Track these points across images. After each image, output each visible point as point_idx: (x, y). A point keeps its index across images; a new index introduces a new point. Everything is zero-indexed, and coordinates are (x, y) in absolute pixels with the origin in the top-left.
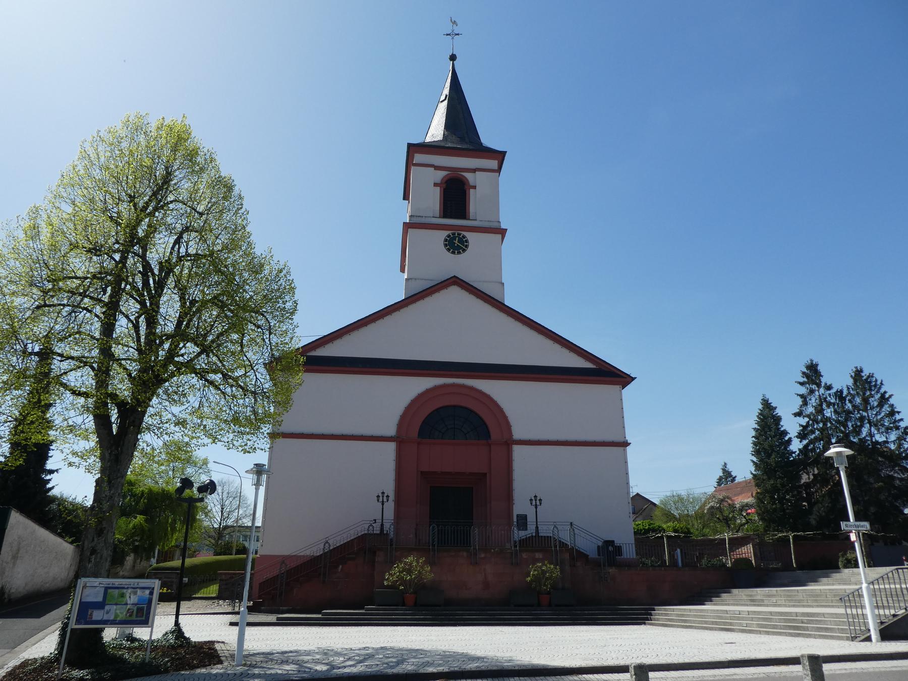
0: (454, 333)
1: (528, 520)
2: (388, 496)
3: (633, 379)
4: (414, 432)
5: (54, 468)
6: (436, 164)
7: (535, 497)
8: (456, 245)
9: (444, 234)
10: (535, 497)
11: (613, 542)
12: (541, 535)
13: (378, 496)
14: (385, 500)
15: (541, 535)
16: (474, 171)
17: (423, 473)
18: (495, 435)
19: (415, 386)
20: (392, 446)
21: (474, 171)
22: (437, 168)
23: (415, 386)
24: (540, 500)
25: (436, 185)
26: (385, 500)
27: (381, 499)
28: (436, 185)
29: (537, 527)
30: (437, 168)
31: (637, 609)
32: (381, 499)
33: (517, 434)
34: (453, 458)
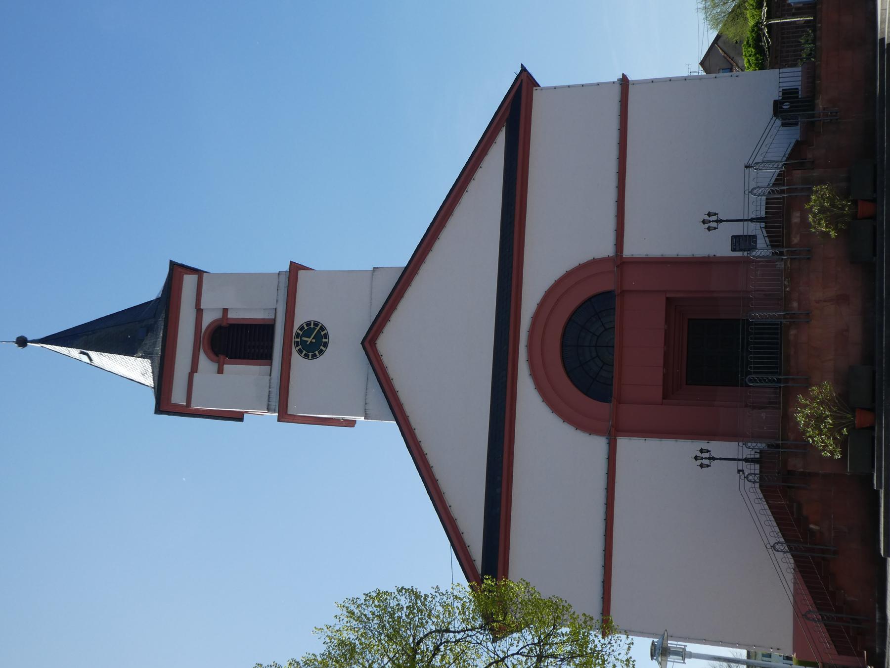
0: (449, 346)
3: (524, 69)
4: (603, 409)
6: (188, 369)
7: (696, 458)
8: (313, 340)
9: (297, 359)
10: (704, 222)
11: (776, 102)
12: (758, 456)
14: (714, 218)
15: (763, 214)
16: (199, 311)
17: (665, 396)
18: (607, 284)
20: (624, 444)
21: (199, 311)
22: (194, 368)
24: (709, 215)
25: (220, 371)
28: (220, 371)
29: (752, 220)
30: (194, 368)
33: (607, 249)
34: (642, 349)
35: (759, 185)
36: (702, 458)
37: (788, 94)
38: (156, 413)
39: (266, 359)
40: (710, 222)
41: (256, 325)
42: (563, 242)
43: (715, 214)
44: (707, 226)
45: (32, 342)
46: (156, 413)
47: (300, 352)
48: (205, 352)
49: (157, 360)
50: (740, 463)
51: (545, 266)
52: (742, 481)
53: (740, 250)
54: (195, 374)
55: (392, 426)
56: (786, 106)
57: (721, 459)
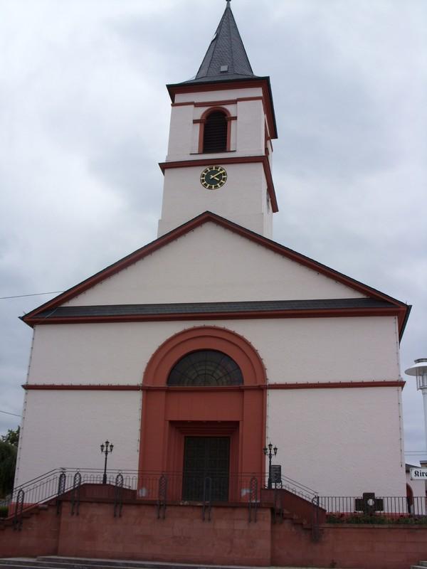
0: (213, 274)
1: (283, 472)
2: (112, 446)
3: (22, 318)
4: (163, 384)
5: (17, 429)
6: (196, 101)
7: (107, 443)
9: (200, 171)
10: (107, 443)
11: (373, 494)
12: (108, 483)
13: (102, 446)
14: (273, 452)
16: (234, 102)
17: (171, 422)
19: (165, 331)
20: (138, 396)
21: (234, 102)
23: (165, 331)
24: (275, 449)
25: (235, 118)
26: (273, 452)
27: (105, 449)
28: (195, 122)
31: (64, 561)
32: (105, 449)
33: (272, 378)
35: (125, 480)
36: (107, 446)
37: (379, 503)
38: (269, 77)
40: (270, 449)
41: (226, 145)
42: (280, 350)
43: (275, 453)
44: (105, 444)
45: (228, 4)
46: (269, 77)
47: (206, 171)
48: (208, 110)
50: (104, 471)
51: (261, 336)
52: (117, 472)
53: (270, 471)
54: (193, 106)
55: (152, 237)
56: (371, 502)
57: (106, 459)
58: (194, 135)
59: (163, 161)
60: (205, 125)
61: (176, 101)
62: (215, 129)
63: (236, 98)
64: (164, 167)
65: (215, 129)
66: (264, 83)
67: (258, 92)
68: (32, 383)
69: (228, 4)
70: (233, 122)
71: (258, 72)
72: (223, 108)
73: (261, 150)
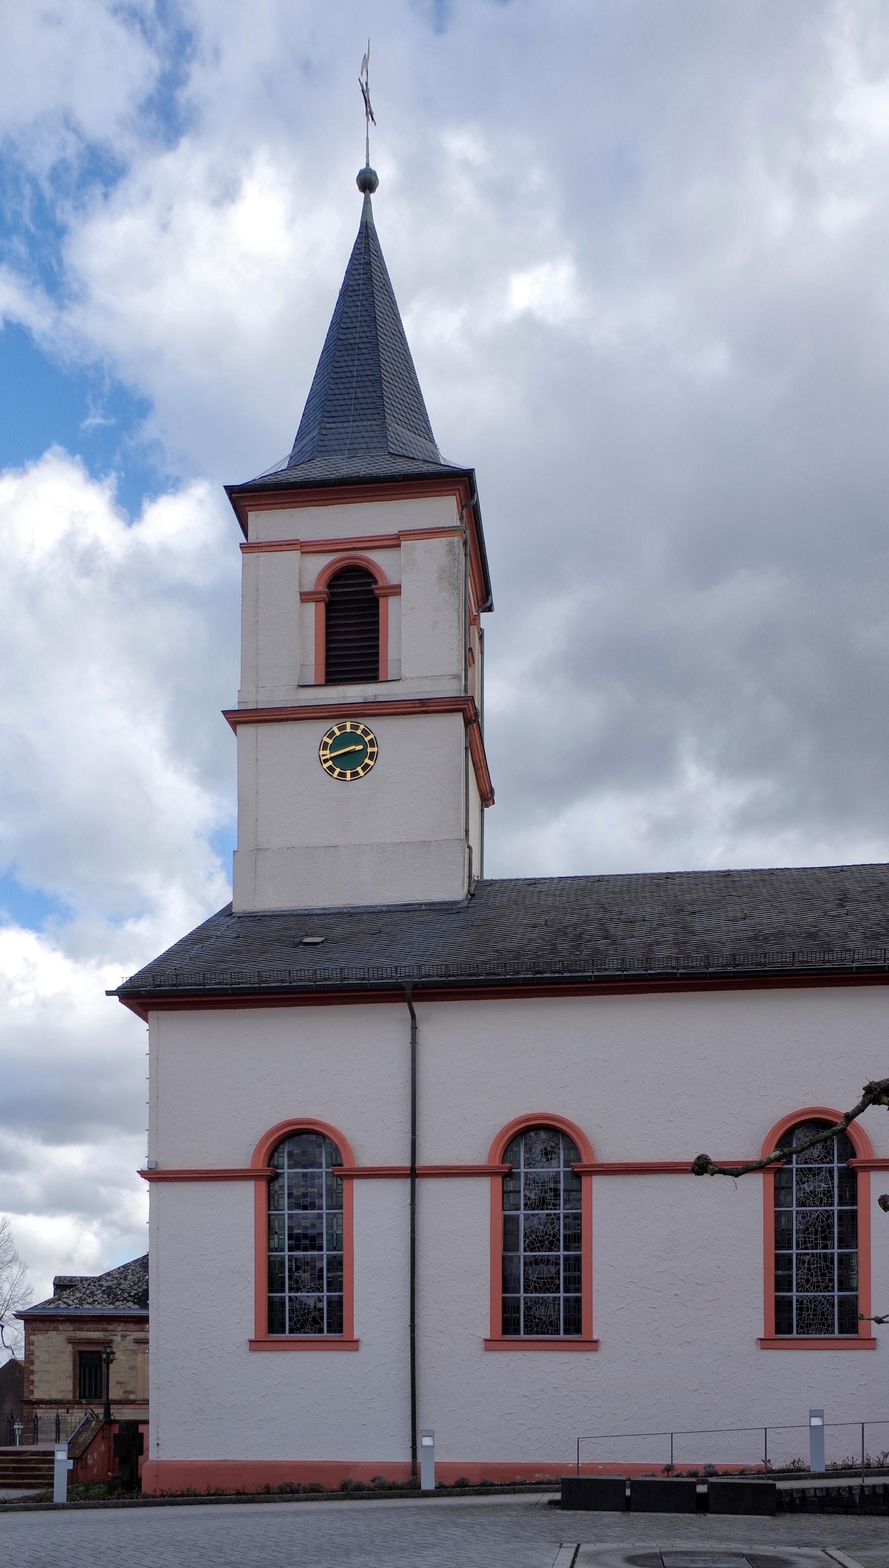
6: (303, 537)
9: (316, 732)
11: (69, 1471)
16: (392, 542)
20: (755, 1187)
21: (392, 542)
22: (307, 548)
30: (307, 548)
39: (327, 673)
45: (367, 203)
49: (298, 475)
58: (301, 634)
59: (233, 705)
60: (322, 605)
61: (252, 539)
62: (351, 617)
63: (394, 530)
64: (237, 718)
65: (351, 617)
66: (461, 482)
67: (443, 510)
68: (169, 1164)
69: (367, 203)
70: (392, 602)
71: (452, 451)
72: (368, 561)
73: (622, 756)
